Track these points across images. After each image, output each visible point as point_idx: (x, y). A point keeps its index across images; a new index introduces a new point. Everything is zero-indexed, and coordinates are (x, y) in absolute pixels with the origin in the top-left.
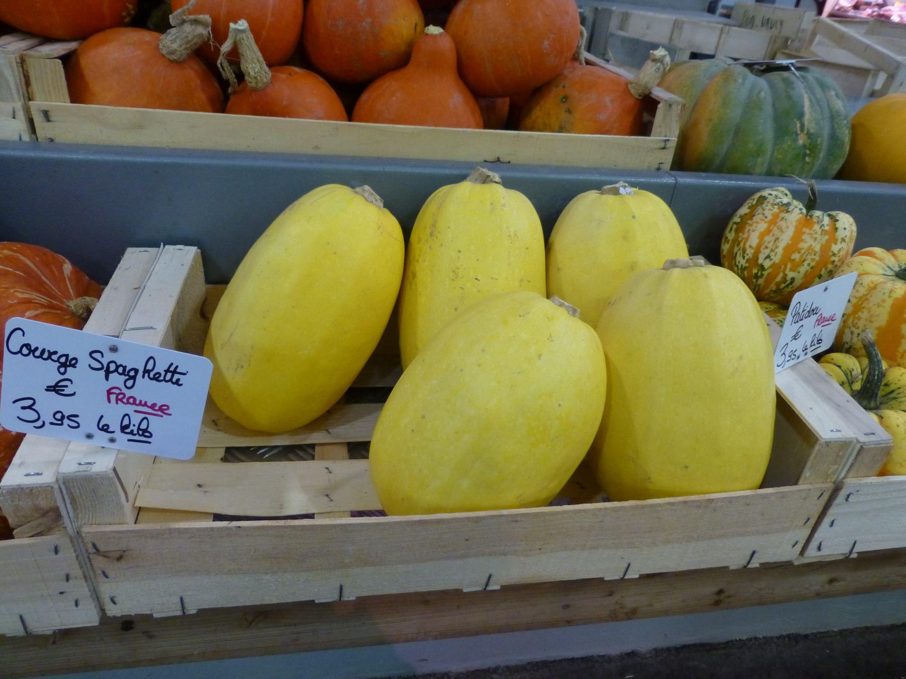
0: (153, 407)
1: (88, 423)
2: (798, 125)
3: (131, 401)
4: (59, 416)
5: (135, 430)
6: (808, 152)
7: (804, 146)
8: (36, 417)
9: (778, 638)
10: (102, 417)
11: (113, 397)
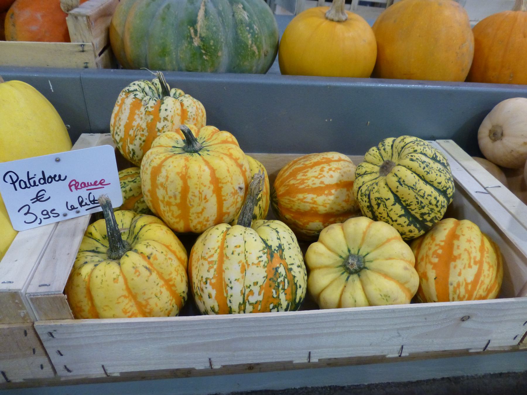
0: (95, 183)
1: (61, 209)
2: (192, 31)
3: (83, 185)
4: (45, 213)
5: (88, 203)
6: (203, 52)
7: (199, 47)
8: (35, 217)
9: (322, 388)
10: (67, 203)
11: (73, 188)
